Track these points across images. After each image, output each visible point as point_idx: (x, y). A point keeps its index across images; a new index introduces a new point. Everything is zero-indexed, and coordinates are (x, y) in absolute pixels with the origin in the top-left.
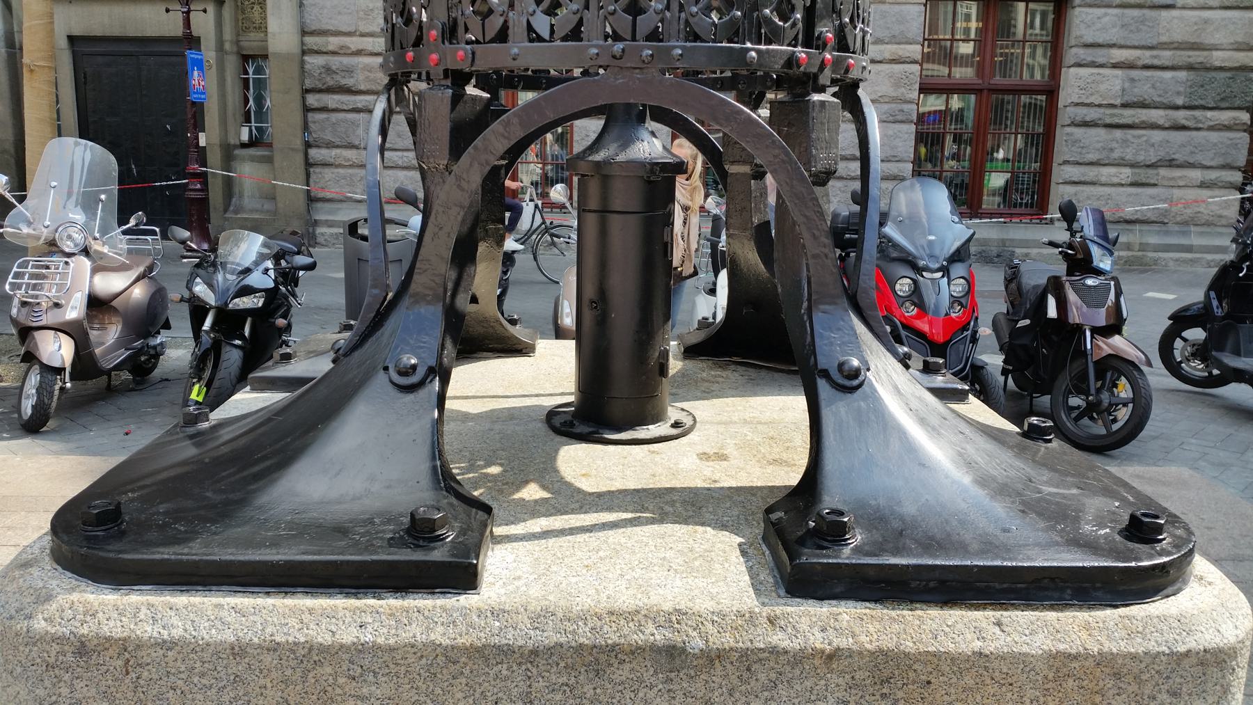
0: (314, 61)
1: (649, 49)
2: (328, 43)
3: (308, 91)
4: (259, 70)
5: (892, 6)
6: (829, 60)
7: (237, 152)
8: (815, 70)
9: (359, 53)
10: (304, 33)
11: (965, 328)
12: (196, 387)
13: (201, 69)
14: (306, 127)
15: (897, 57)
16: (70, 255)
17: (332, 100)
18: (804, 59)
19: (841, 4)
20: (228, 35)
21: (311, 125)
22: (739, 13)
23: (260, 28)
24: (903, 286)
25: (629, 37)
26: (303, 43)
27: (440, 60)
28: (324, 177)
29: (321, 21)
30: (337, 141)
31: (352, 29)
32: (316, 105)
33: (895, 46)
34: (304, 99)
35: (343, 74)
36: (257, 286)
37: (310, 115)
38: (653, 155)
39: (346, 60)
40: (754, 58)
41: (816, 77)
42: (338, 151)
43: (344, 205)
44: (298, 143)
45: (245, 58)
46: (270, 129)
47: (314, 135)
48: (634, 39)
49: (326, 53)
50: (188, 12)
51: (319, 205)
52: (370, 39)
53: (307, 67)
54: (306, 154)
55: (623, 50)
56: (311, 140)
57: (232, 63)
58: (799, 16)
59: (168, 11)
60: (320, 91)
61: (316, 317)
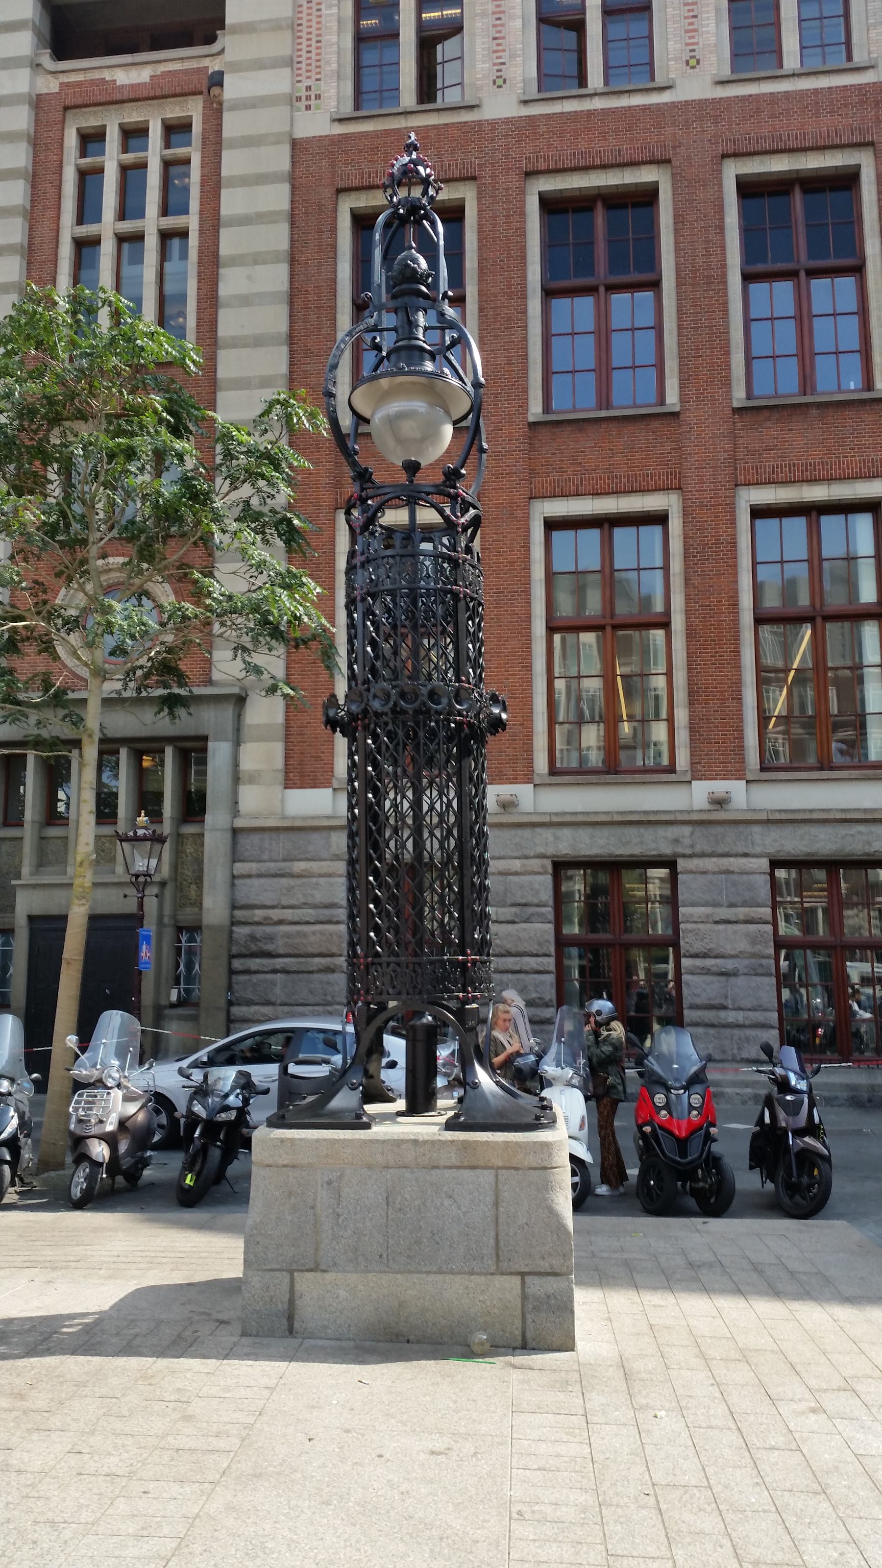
0: (241, 931)
2: (254, 915)
3: (234, 956)
4: (191, 940)
7: (167, 1012)
9: (281, 922)
10: (234, 907)
11: (701, 1128)
12: (189, 1176)
13: (148, 943)
14: (230, 988)
16: (111, 1088)
17: (255, 963)
20: (167, 910)
21: (236, 987)
24: (660, 1099)
26: (232, 916)
31: (275, 903)
33: (747, 909)
34: (230, 963)
36: (232, 1105)
37: (235, 978)
39: (268, 929)
42: (256, 1008)
44: (222, 1003)
45: (180, 929)
50: (142, 898)
52: (290, 911)
53: (235, 936)
57: (169, 934)
59: (125, 896)
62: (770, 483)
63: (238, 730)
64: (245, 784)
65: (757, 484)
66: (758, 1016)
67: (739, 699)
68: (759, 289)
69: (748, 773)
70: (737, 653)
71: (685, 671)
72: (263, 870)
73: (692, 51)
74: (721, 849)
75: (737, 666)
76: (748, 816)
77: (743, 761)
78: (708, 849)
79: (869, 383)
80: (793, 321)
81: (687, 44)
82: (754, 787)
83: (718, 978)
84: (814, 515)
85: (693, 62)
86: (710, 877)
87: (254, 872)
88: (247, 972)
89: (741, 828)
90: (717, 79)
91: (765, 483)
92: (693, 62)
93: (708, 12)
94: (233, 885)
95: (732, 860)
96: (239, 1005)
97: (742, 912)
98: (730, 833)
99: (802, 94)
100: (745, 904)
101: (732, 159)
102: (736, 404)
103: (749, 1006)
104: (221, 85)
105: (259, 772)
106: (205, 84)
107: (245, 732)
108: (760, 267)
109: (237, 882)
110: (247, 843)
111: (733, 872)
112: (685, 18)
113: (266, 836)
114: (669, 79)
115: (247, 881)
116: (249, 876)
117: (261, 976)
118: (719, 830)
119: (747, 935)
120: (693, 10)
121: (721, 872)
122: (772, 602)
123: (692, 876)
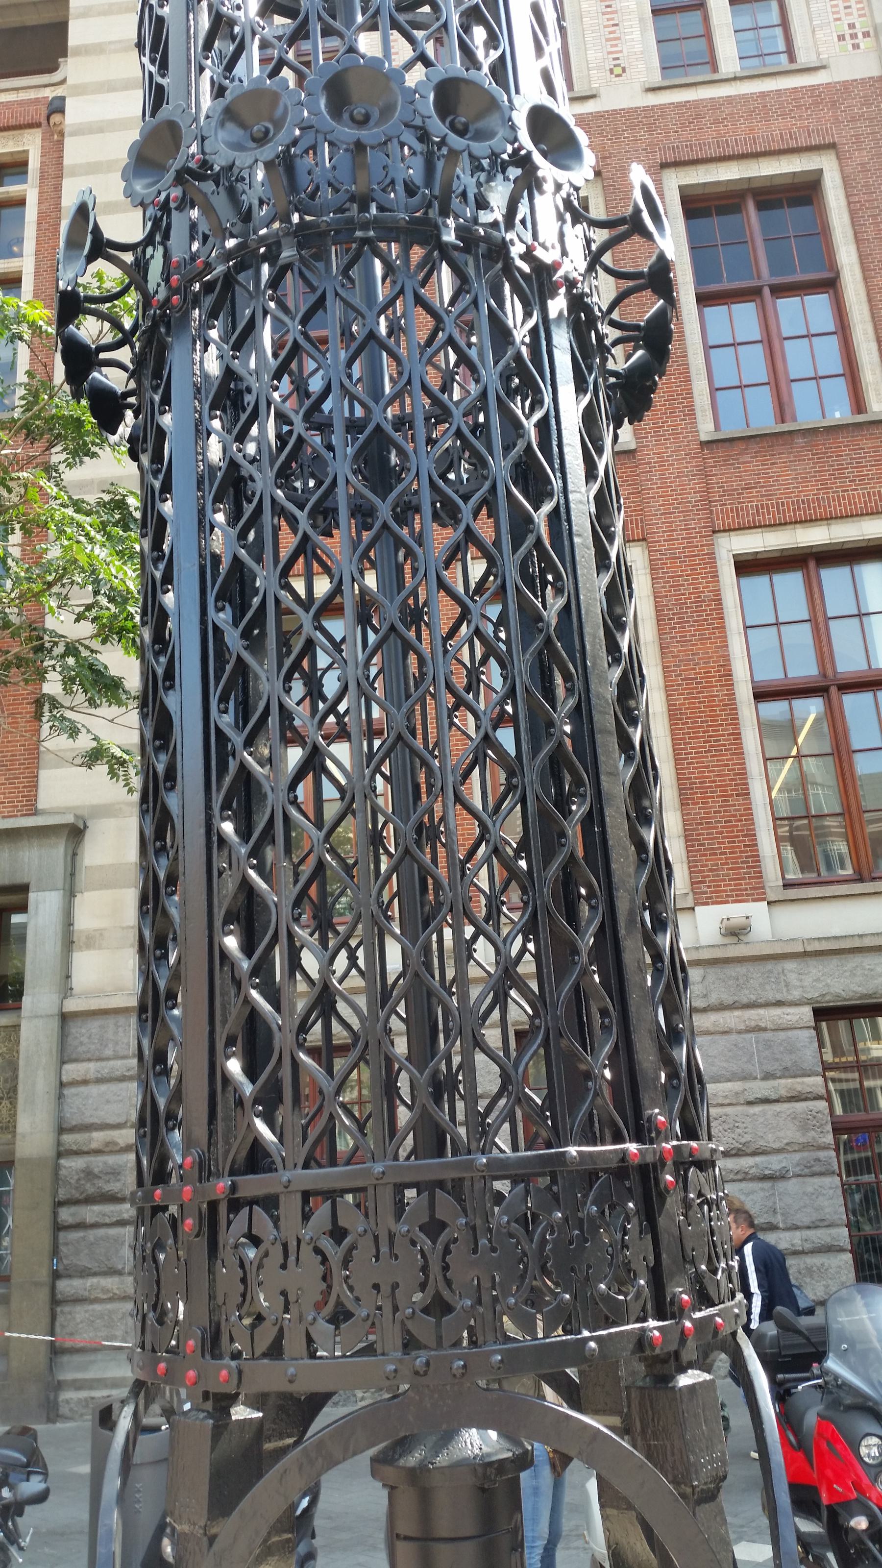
1: (460, 1359)
3: (61, 1204)
5: (775, 1033)
6: (690, 1329)
8: (673, 1347)
10: (61, 1130)
14: (55, 1251)
15: (795, 1094)
17: (91, 1213)
18: (657, 1339)
19: (693, 1250)
21: (63, 1249)
22: (568, 1296)
23: (7, 1128)
25: (433, 1344)
26: (59, 1143)
27: (199, 1376)
28: (74, 1318)
29: (83, 1114)
30: (93, 1265)
31: (121, 1120)
32: (70, 1220)
33: (790, 1080)
34: (55, 1214)
35: (107, 1178)
37: (62, 1235)
38: (485, 1449)
39: (111, 1160)
40: (594, 1350)
41: (677, 1354)
42: (94, 1280)
43: (99, 1356)
44: (43, 1275)
46: (9, 1258)
47: (65, 1262)
48: (440, 1344)
49: (87, 1153)
51: (66, 1358)
53: (63, 1172)
54: (53, 1288)
55: (428, 1364)
56: (61, 1267)
58: (642, 1282)
60: (76, 1202)
61: (47, 1550)
62: (755, 527)
63: (73, 875)
64: (80, 949)
65: (740, 529)
66: (820, 1236)
67: (745, 794)
68: (717, 313)
69: (768, 891)
70: (737, 736)
71: (672, 763)
72: (105, 1072)
73: (615, 59)
74: (746, 997)
75: (740, 753)
76: (778, 949)
77: (759, 875)
78: (729, 999)
79: (859, 404)
80: (759, 347)
81: (609, 53)
82: (778, 910)
83: (760, 1185)
84: (812, 564)
85: (618, 71)
86: (734, 1037)
87: (92, 1075)
88: (81, 1226)
89: (770, 965)
90: (647, 86)
91: (750, 528)
92: (618, 71)
93: (630, 20)
94: (60, 1096)
95: (762, 1011)
96: (70, 1276)
97: (783, 1086)
98: (755, 972)
99: (745, 99)
100: (787, 1073)
101: (673, 170)
102: (704, 437)
103: (806, 1221)
104: (62, 111)
105: (101, 932)
106: (44, 112)
107: (82, 878)
108: (714, 287)
109: (66, 1092)
110: (80, 1031)
111: (765, 1029)
112: (605, 27)
113: (111, 1021)
114: (591, 89)
115: (82, 1089)
116: (85, 1082)
117: (101, 1232)
118: (740, 970)
119: (794, 1117)
120: (612, 19)
121: (749, 1030)
122: (772, 674)
123: (709, 1038)
